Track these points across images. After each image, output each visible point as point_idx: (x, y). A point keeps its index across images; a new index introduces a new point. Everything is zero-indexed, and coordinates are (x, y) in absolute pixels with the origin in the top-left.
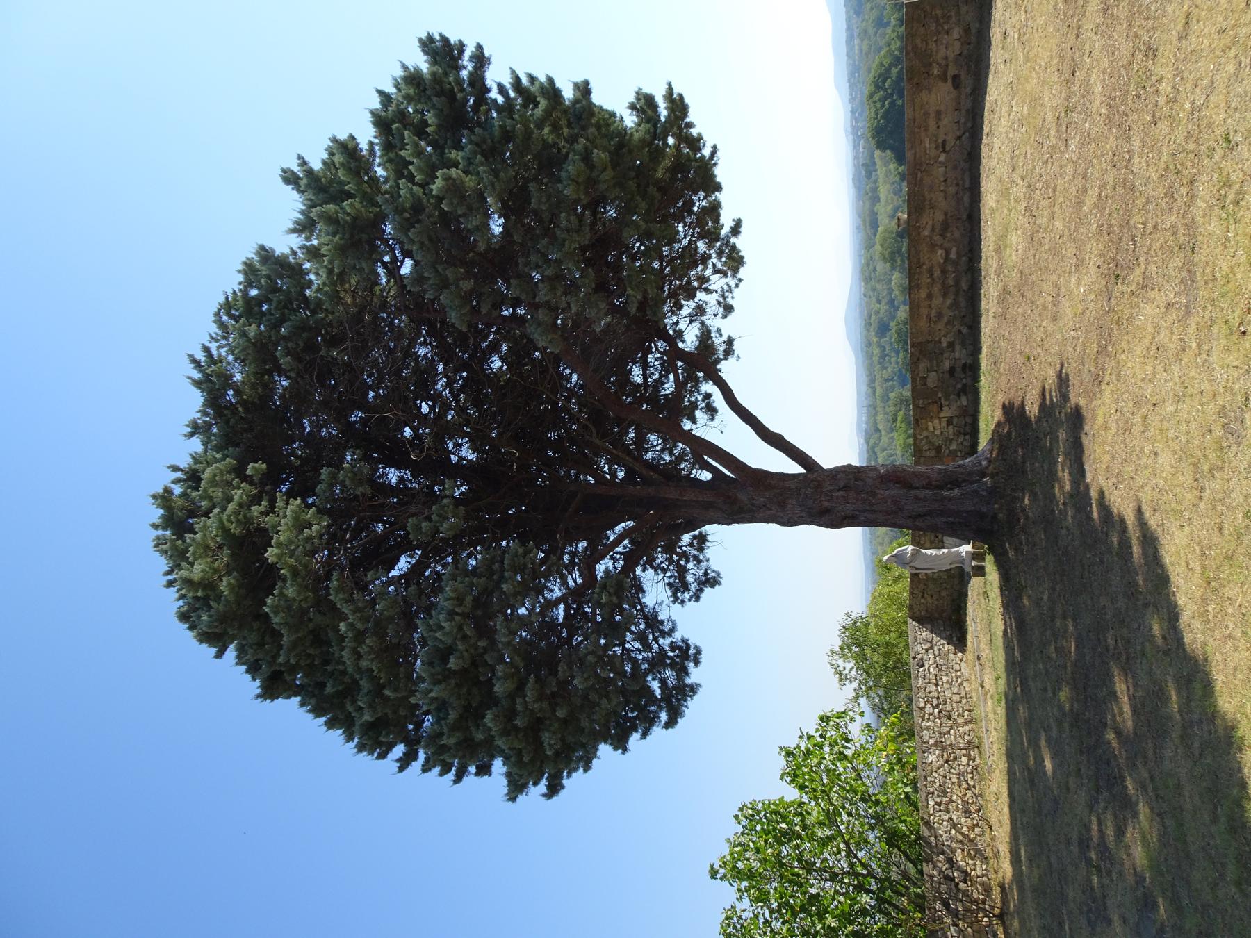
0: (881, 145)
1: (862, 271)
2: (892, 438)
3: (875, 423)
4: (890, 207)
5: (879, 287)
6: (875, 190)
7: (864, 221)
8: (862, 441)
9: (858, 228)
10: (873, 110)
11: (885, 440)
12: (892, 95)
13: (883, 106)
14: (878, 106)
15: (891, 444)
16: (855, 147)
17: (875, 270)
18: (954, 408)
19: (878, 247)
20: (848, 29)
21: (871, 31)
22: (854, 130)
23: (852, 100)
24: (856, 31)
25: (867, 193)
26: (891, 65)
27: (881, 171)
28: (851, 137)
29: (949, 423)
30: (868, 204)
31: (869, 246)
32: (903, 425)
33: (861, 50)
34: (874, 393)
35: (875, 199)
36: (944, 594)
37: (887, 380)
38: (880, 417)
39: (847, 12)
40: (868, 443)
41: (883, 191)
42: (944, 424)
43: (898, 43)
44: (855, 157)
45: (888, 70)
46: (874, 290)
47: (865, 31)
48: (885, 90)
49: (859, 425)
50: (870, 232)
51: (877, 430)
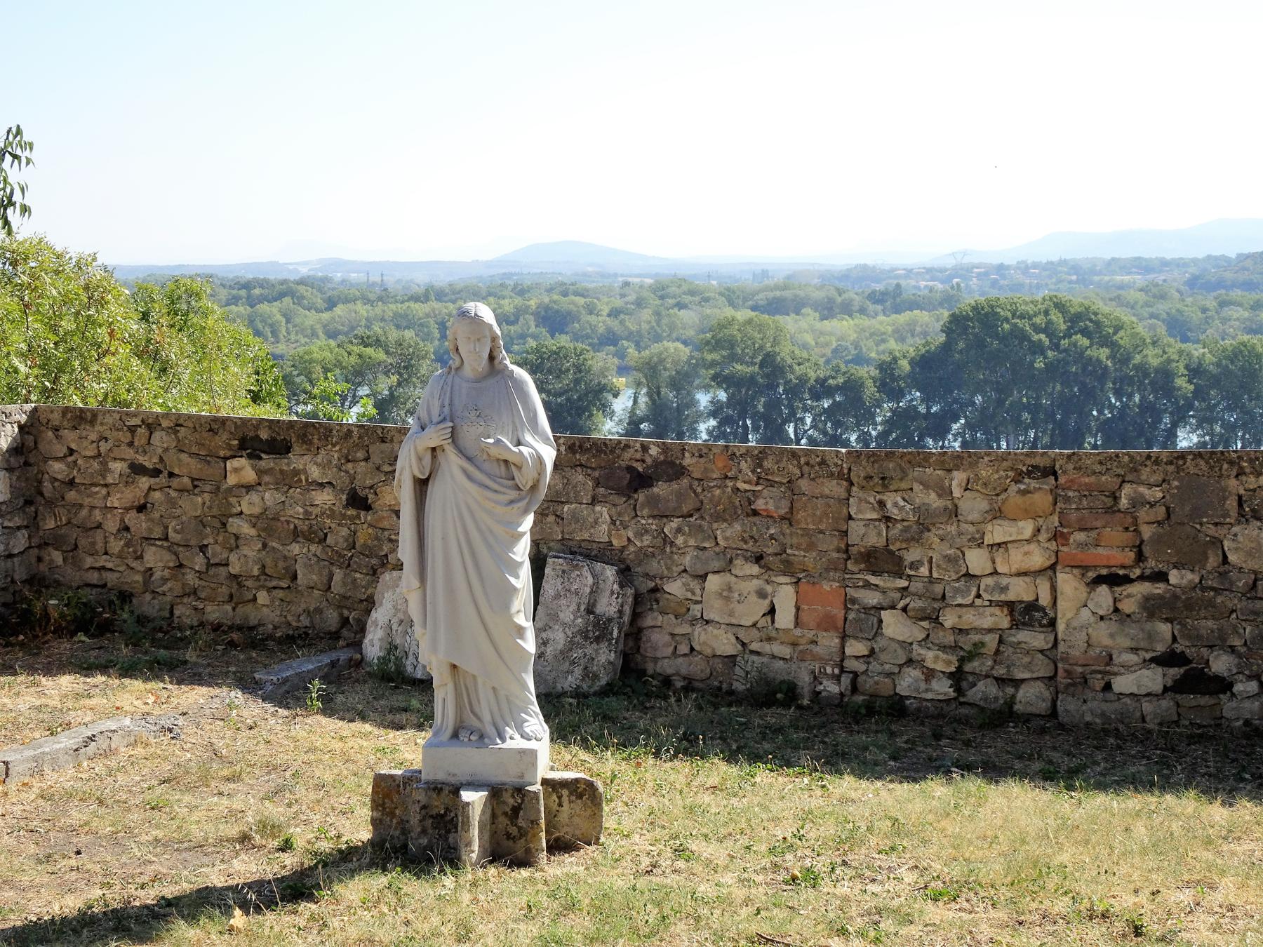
0: (957, 325)
1: (680, 281)
2: (314, 334)
3: (347, 300)
4: (809, 339)
5: (646, 314)
6: (847, 309)
7: (785, 287)
8: (304, 271)
9: (765, 273)
10: (1030, 309)
11: (311, 319)
12: (1056, 346)
13: (1037, 329)
14: (1038, 320)
15: (302, 331)
16: (930, 272)
17: (681, 306)
18: (1103, 635)
19: (742, 315)
20: (1165, 264)
21: (1162, 307)
22: (963, 271)
23: (1024, 268)
24: (1160, 278)
25: (836, 297)
26: (1113, 345)
27: (884, 322)
28: (950, 263)
29: (1026, 614)
30: (819, 295)
31: (732, 296)
32: (353, 359)
33: (1121, 287)
34: (415, 298)
35: (828, 309)
36: (155, 558)
37: (443, 326)
38: (363, 310)
39: (1195, 261)
40: (302, 282)
41: (843, 327)
42: (1020, 591)
43: (1155, 362)
44: (909, 272)
45: (1106, 341)
46: (640, 303)
47: (1163, 297)
48: (1068, 335)
49: (339, 264)
50: (761, 298)
51: (331, 304)
